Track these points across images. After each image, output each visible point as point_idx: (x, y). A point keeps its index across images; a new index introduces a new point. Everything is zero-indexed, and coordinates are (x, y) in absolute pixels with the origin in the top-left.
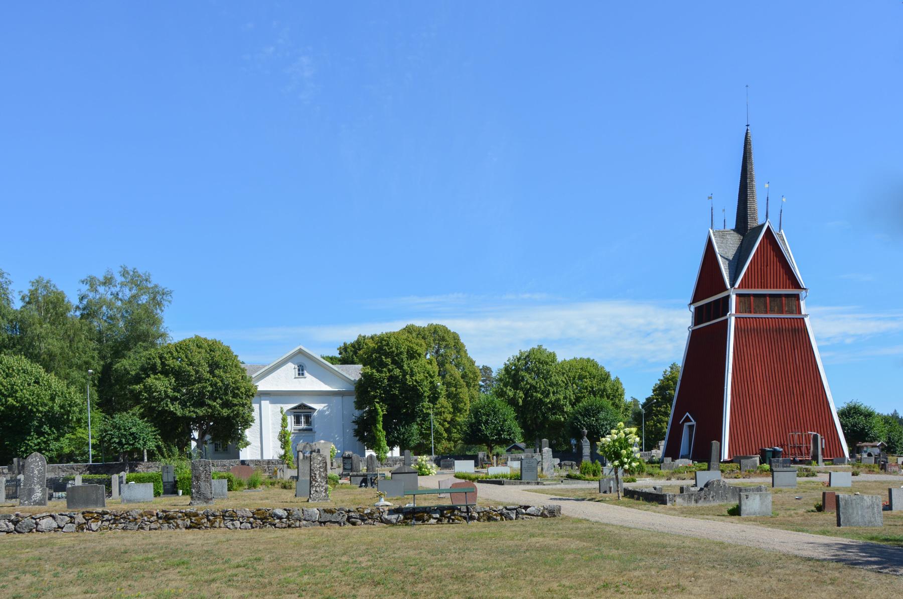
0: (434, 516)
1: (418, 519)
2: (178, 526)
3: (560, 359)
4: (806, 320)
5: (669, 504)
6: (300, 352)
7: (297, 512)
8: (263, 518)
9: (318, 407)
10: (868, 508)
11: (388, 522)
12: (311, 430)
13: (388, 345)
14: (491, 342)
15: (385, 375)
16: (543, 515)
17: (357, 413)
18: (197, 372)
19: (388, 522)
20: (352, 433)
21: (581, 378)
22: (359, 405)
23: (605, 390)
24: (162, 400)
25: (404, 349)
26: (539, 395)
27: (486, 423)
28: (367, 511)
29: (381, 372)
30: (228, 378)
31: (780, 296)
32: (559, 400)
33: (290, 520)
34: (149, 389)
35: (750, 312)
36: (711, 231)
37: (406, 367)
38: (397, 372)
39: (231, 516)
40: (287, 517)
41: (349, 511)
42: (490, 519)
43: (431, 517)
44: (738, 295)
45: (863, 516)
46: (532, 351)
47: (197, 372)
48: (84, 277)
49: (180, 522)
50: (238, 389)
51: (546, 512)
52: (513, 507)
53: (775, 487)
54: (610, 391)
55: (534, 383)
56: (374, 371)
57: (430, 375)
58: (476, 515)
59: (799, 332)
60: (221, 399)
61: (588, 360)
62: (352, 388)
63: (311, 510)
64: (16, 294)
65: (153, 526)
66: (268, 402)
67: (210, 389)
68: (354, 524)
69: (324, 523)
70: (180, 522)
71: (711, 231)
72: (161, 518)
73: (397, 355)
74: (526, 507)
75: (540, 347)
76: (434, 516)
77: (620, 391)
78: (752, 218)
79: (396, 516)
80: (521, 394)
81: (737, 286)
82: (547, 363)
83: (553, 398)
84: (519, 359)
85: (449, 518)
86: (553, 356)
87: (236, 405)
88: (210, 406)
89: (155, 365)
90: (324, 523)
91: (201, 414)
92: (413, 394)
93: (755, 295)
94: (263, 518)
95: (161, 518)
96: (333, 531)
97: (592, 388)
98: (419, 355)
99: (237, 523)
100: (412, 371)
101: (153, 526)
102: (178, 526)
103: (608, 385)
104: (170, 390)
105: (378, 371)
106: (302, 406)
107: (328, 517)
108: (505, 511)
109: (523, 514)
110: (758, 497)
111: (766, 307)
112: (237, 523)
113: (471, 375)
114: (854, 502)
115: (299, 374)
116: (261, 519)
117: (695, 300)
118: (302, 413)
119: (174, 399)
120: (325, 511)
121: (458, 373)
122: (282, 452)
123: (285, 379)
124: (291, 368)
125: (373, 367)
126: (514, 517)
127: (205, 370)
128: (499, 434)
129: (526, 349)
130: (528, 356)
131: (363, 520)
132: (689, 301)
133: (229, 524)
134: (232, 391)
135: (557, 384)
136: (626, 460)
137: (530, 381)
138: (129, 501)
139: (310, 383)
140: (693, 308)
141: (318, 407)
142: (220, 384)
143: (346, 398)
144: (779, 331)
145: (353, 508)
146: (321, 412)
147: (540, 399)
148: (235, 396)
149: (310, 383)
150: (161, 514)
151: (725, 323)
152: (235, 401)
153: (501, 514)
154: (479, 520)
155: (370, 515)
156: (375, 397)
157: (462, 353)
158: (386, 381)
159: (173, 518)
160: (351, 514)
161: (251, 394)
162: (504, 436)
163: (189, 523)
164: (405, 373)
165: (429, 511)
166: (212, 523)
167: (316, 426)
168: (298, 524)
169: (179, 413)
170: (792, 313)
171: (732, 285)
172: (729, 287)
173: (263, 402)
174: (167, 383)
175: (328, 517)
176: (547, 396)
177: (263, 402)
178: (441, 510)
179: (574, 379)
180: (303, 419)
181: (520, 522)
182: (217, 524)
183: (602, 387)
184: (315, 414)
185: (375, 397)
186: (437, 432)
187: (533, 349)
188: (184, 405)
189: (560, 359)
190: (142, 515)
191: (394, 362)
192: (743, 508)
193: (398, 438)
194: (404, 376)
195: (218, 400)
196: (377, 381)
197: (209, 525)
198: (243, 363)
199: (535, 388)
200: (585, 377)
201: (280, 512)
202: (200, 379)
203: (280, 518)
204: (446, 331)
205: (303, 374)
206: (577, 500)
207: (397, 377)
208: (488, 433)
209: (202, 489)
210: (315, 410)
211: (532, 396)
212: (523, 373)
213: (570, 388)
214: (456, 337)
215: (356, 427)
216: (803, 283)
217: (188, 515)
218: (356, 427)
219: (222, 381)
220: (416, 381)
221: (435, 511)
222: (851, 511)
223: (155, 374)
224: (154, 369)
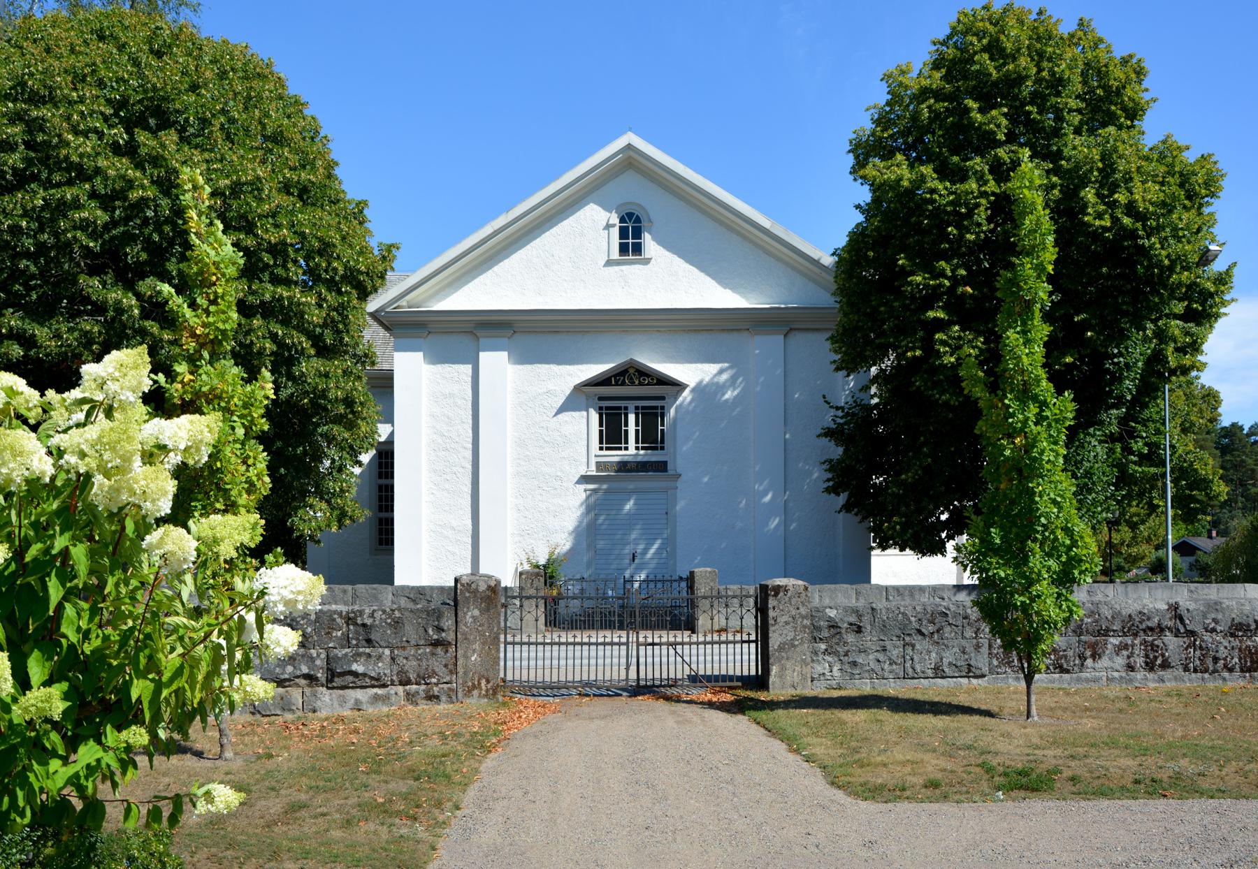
6: (631, 161)
13: (995, 49)
17: (846, 387)
20: (818, 476)
25: (1068, 64)
48: (819, 431)
56: (927, 170)
62: (825, 298)
105: (944, 172)
115: (623, 249)
118: (627, 402)
122: (300, 632)
124: (594, 225)
143: (798, 339)
149: (670, 281)
158: (981, 215)
167: (684, 449)
173: (485, 357)
177: (485, 357)
185: (929, 301)
186: (1184, 473)
196: (940, 217)
205: (638, 249)
210: (678, 386)
215: (837, 452)
218: (837, 452)
220: (1131, 209)
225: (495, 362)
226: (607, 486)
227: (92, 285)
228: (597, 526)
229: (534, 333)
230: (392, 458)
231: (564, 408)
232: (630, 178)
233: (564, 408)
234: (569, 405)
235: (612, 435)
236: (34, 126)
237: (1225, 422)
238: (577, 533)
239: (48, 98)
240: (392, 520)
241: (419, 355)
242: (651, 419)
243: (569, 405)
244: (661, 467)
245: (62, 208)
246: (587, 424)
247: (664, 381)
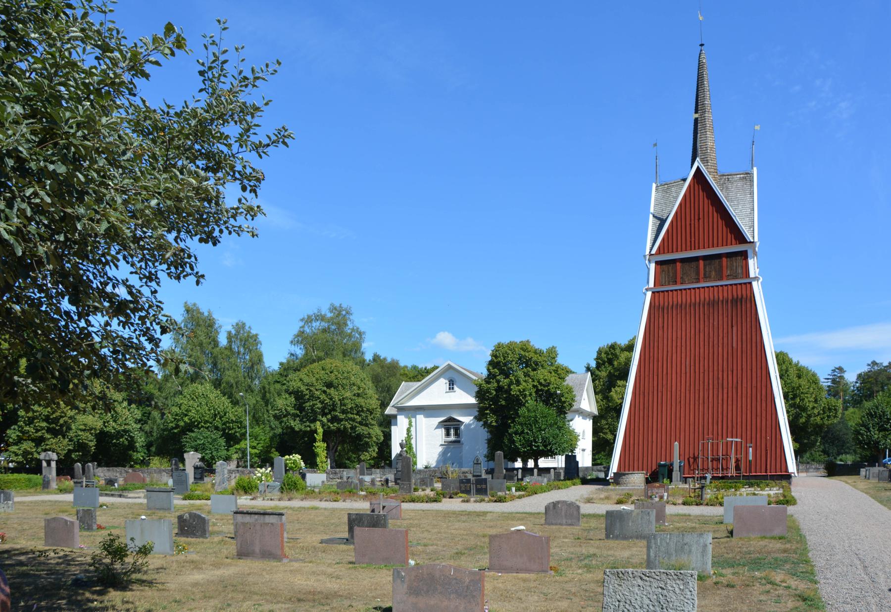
4: (754, 284)
31: (719, 256)
35: (675, 283)
59: (744, 303)
66: (422, 416)
67: (319, 405)
73: (505, 364)
87: (342, 420)
93: (683, 261)
106: (451, 419)
111: (698, 273)
118: (450, 425)
123: (437, 393)
124: (443, 383)
144: (713, 304)
152: (342, 416)
170: (736, 277)
180: (452, 432)
184: (462, 427)
202: (312, 397)
210: (462, 423)
216: (749, 236)
225: (420, 418)
228: (444, 457)
229: (428, 410)
230: (390, 439)
231: (436, 428)
232: (451, 371)
233: (436, 428)
234: (437, 427)
235: (448, 434)
236: (311, 391)
238: (573, 431)
239: (312, 385)
240: (390, 435)
242: (457, 430)
243: (437, 427)
244: (458, 442)
245: (314, 405)
246: (442, 431)
247: (459, 421)
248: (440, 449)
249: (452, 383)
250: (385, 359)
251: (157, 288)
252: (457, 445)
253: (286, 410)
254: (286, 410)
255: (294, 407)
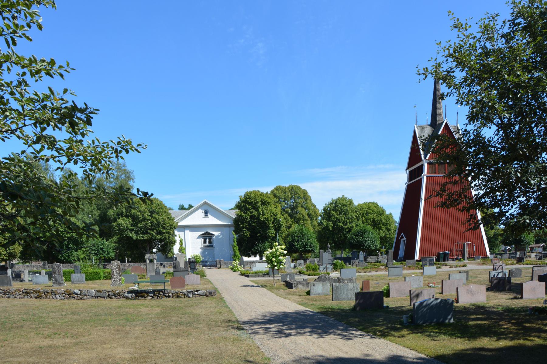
0: (150, 295)
1: (142, 297)
2: (31, 297)
3: (356, 203)
5: (294, 289)
7: (85, 292)
8: (69, 294)
9: (216, 233)
10: (351, 290)
11: (127, 298)
12: (212, 246)
13: (250, 198)
14: (321, 195)
15: (248, 215)
16: (206, 295)
18: (143, 215)
19: (127, 298)
21: (367, 213)
22: (236, 232)
23: (381, 220)
24: (126, 231)
25: (259, 200)
26: (341, 224)
27: (298, 241)
28: (117, 292)
29: (246, 213)
30: (160, 218)
32: (353, 227)
33: (82, 296)
34: (118, 226)
36: (416, 126)
37: (260, 211)
38: (255, 213)
39: (54, 293)
40: (80, 294)
41: (109, 292)
42: (178, 297)
43: (148, 296)
44: (428, 164)
45: (347, 295)
46: (339, 199)
47: (143, 215)
49: (32, 295)
50: (165, 224)
51: (208, 294)
52: (190, 290)
53: (441, 280)
54: (384, 221)
55: (338, 217)
57: (274, 215)
58: (171, 295)
60: (157, 230)
61: (373, 203)
63: (91, 290)
64: (57, 177)
65: (21, 296)
68: (111, 298)
69: (97, 297)
70: (32, 295)
71: (416, 126)
72: (23, 293)
73: (255, 203)
74: (197, 291)
75: (343, 196)
76: (150, 295)
77: (391, 221)
78: (439, 118)
79: (130, 295)
80: (331, 224)
81: (427, 158)
82: (346, 206)
83: (349, 225)
84: (331, 204)
85: (158, 296)
86: (351, 202)
87: (164, 233)
88: (150, 234)
89: (122, 212)
90: (97, 297)
91: (146, 238)
92: (264, 225)
94: (69, 294)
95: (23, 293)
96: (101, 301)
97: (374, 219)
98: (269, 203)
99: (58, 296)
100: (263, 212)
101: (21, 296)
102: (31, 297)
103: (382, 217)
104: (129, 226)
105: (244, 213)
106: (207, 233)
107: (99, 294)
108: (186, 293)
109: (196, 294)
110: (321, 285)
112: (58, 296)
113: (313, 213)
114: (342, 287)
116: (68, 295)
117: (409, 167)
118: (207, 237)
119: (132, 230)
120: (97, 291)
121: (305, 213)
123: (197, 218)
124: (201, 212)
125: (242, 211)
126: (191, 296)
127: (147, 215)
128: (305, 247)
129: (335, 197)
130: (336, 202)
131: (115, 296)
132: (406, 167)
133: (54, 297)
134: (162, 226)
135: (352, 218)
136: (276, 264)
137: (336, 216)
138: (36, 284)
139: (212, 220)
140: (408, 171)
141: (216, 233)
142: (155, 222)
145: (111, 290)
146: (218, 236)
147: (342, 227)
148: (164, 228)
149: (212, 220)
150: (24, 291)
151: (421, 181)
152: (164, 231)
153: (185, 295)
154: (173, 297)
155: (119, 294)
156: (243, 228)
157: (308, 201)
159: (29, 293)
160: (110, 293)
161: (173, 227)
162: (308, 248)
163: (36, 296)
164: (259, 214)
165: (147, 292)
166: (46, 296)
168: (85, 297)
169: (134, 238)
171: (425, 158)
172: (423, 158)
174: (127, 222)
175: (99, 294)
176: (346, 224)
178: (154, 291)
179: (363, 214)
180: (208, 240)
181: (195, 299)
182: (48, 297)
183: (379, 219)
185: (243, 228)
187: (339, 198)
188: (137, 233)
189: (356, 203)
190: (15, 291)
191: (253, 208)
192: (312, 291)
193: (257, 250)
194: (259, 215)
195: (155, 231)
197: (44, 296)
198: (170, 209)
199: (339, 220)
200: (370, 213)
201: (77, 291)
202: (145, 219)
203: (77, 294)
204: (299, 188)
206: (244, 286)
207: (255, 216)
208: (298, 247)
209: (58, 279)
210: (214, 235)
211: (337, 225)
212: (332, 212)
213: (360, 220)
214: (305, 192)
217: (36, 292)
219: (156, 220)
220: (265, 218)
221: (151, 292)
222: (339, 292)
223: (122, 217)
224: (122, 214)
225: (187, 232)
226: (205, 248)
227: (149, 231)
229: (193, 228)
235: (205, 242)
237: (320, 208)
241: (331, 336)
246: (201, 240)
247: (212, 234)
248: (201, 250)
249: (206, 213)
250: (267, 193)
251: (464, 105)
252: (211, 248)
253: (127, 227)
254: (127, 227)
255: (132, 225)
